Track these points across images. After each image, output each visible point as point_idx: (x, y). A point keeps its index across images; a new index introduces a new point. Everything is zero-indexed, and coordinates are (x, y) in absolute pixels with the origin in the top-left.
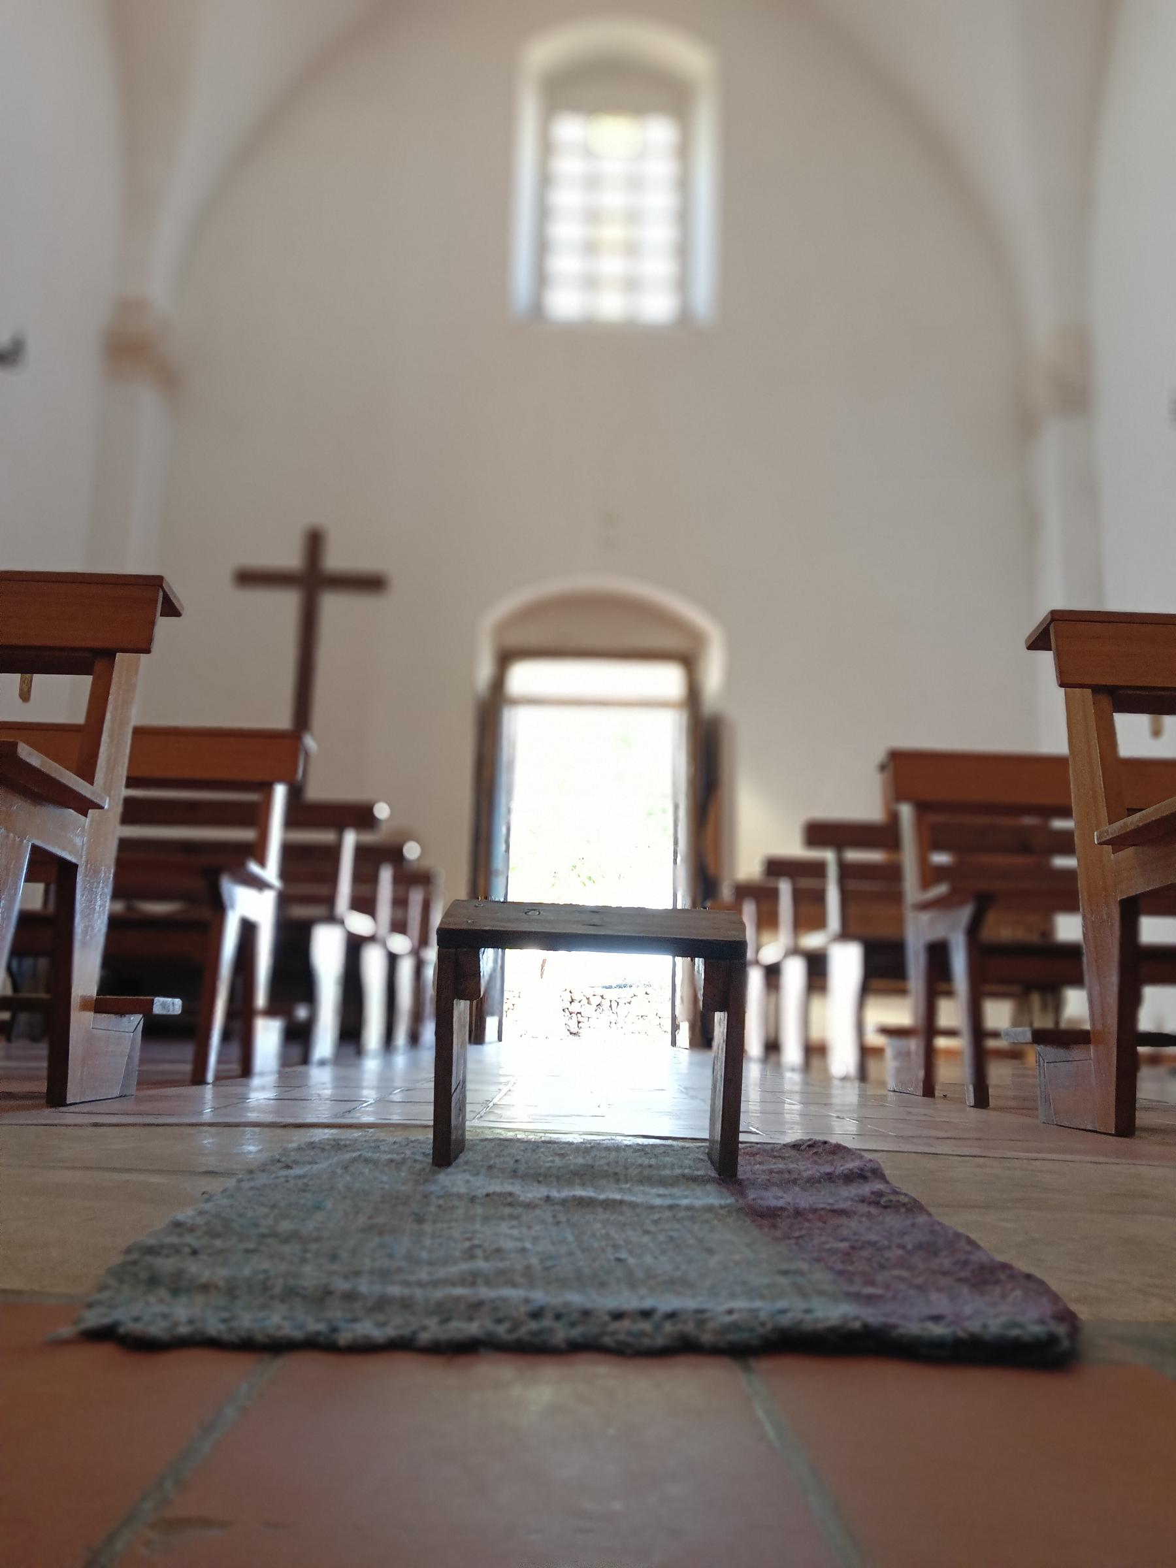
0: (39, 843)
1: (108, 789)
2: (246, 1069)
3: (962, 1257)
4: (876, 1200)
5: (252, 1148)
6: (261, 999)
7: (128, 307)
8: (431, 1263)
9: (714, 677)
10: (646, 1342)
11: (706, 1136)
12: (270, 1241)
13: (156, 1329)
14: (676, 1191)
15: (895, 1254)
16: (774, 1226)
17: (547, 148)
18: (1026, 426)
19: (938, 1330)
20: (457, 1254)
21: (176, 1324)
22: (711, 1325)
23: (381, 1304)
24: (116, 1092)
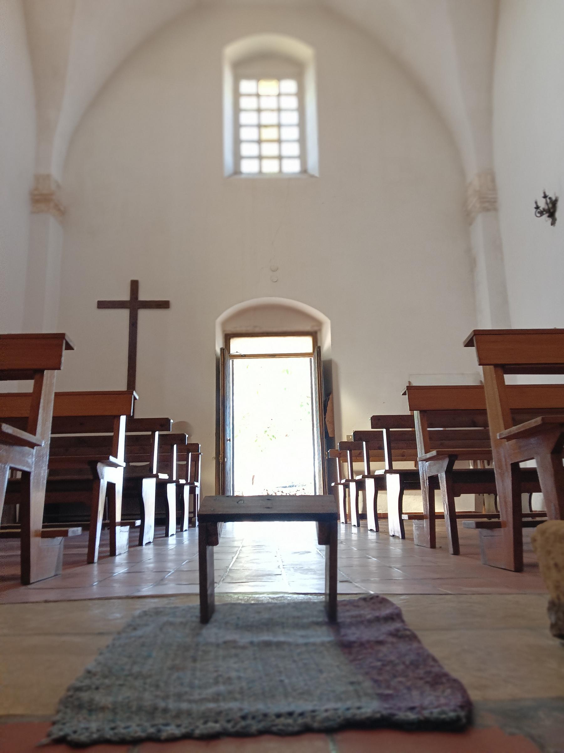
0: (13, 465)
1: (43, 434)
2: (113, 553)
3: (428, 669)
4: (395, 634)
5: (118, 615)
6: (118, 518)
7: (41, 179)
8: (200, 687)
9: (327, 342)
10: (290, 729)
11: (323, 592)
12: (129, 678)
13: (83, 737)
14: (309, 632)
15: (401, 667)
16: (350, 653)
17: (237, 95)
18: (468, 218)
19: (412, 716)
20: (211, 681)
21: (92, 733)
22: (318, 718)
23: (179, 714)
24: (53, 574)
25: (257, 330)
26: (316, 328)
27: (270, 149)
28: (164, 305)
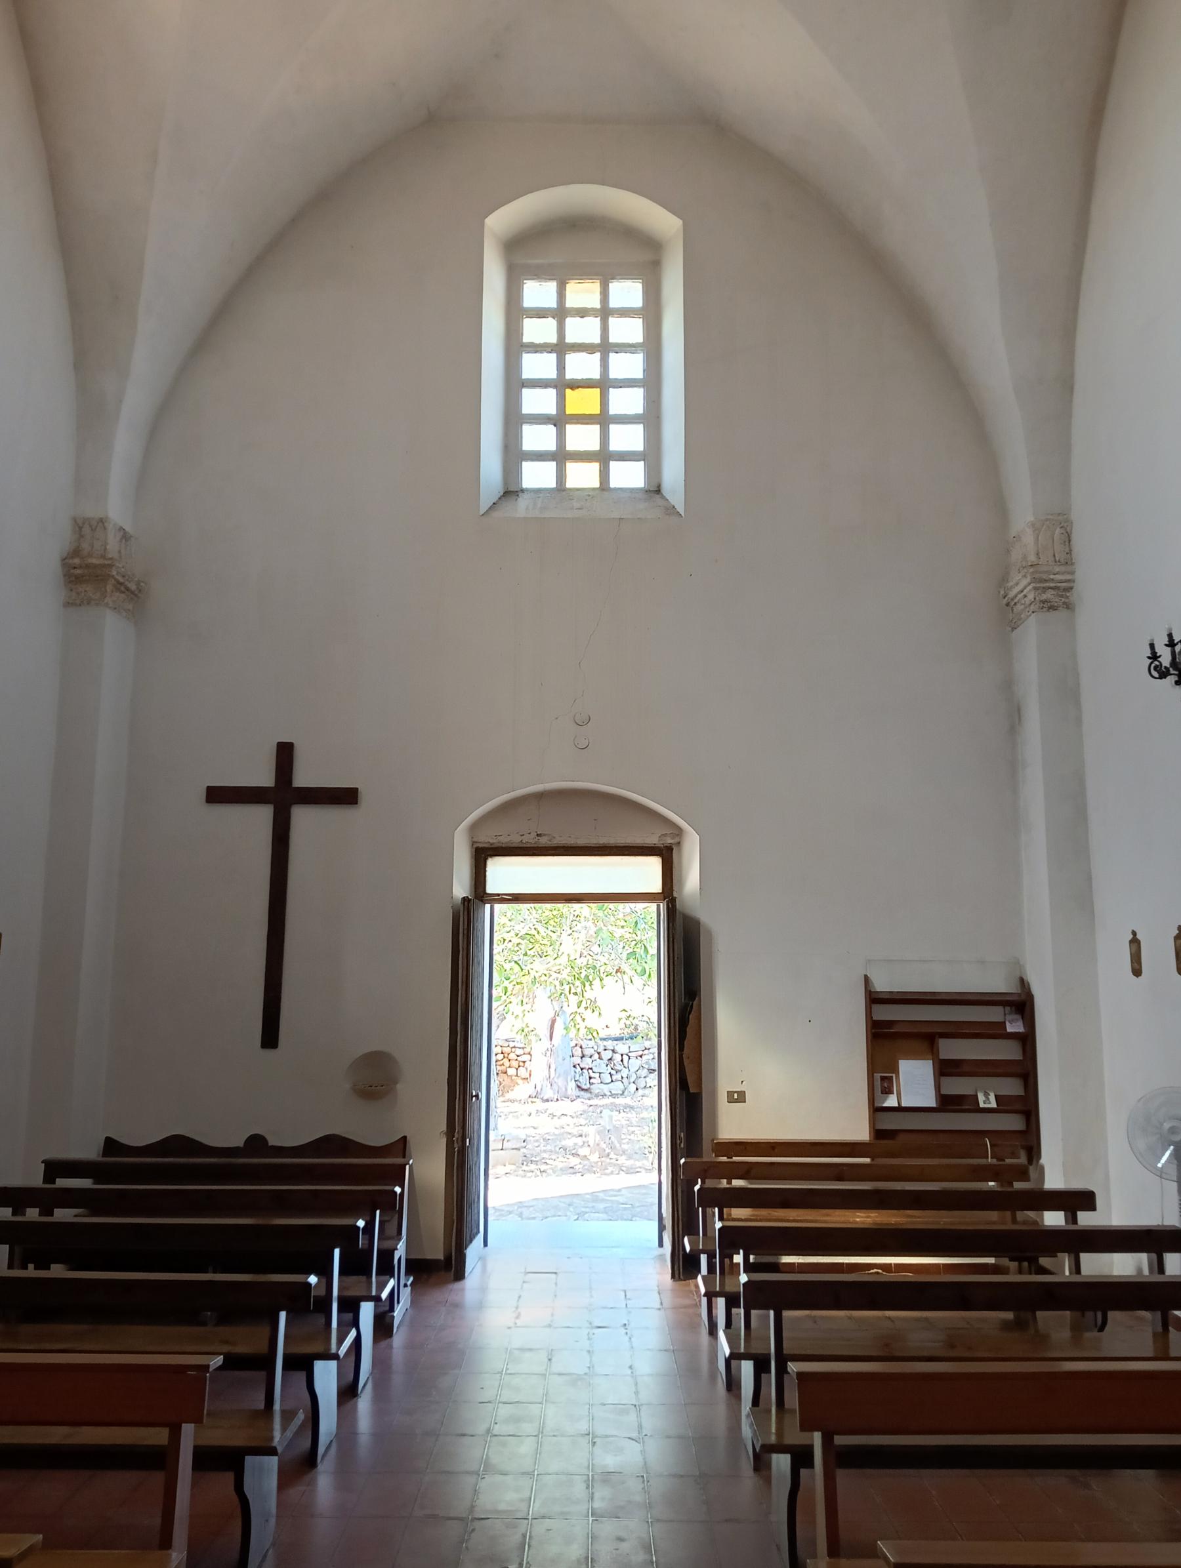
7: (86, 527)
9: (691, 880)
17: (515, 312)
18: (1008, 615)
25: (544, 841)
26: (669, 841)
27: (583, 330)
28: (347, 797)
